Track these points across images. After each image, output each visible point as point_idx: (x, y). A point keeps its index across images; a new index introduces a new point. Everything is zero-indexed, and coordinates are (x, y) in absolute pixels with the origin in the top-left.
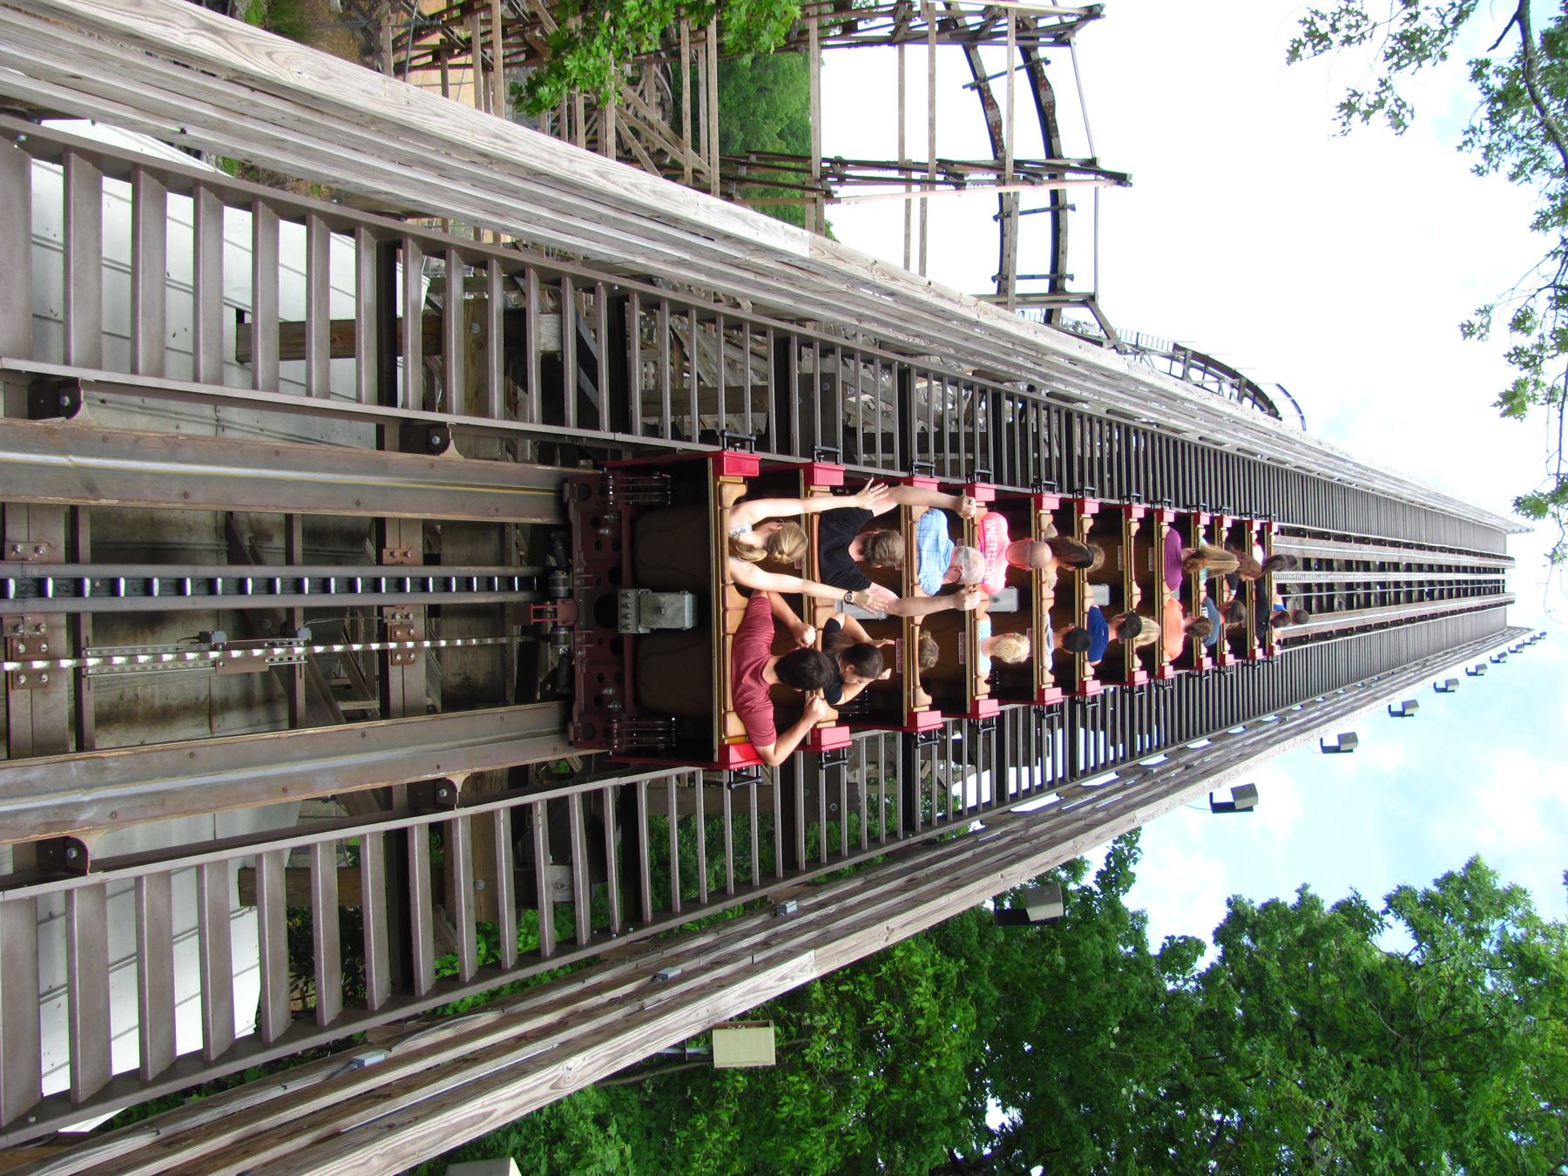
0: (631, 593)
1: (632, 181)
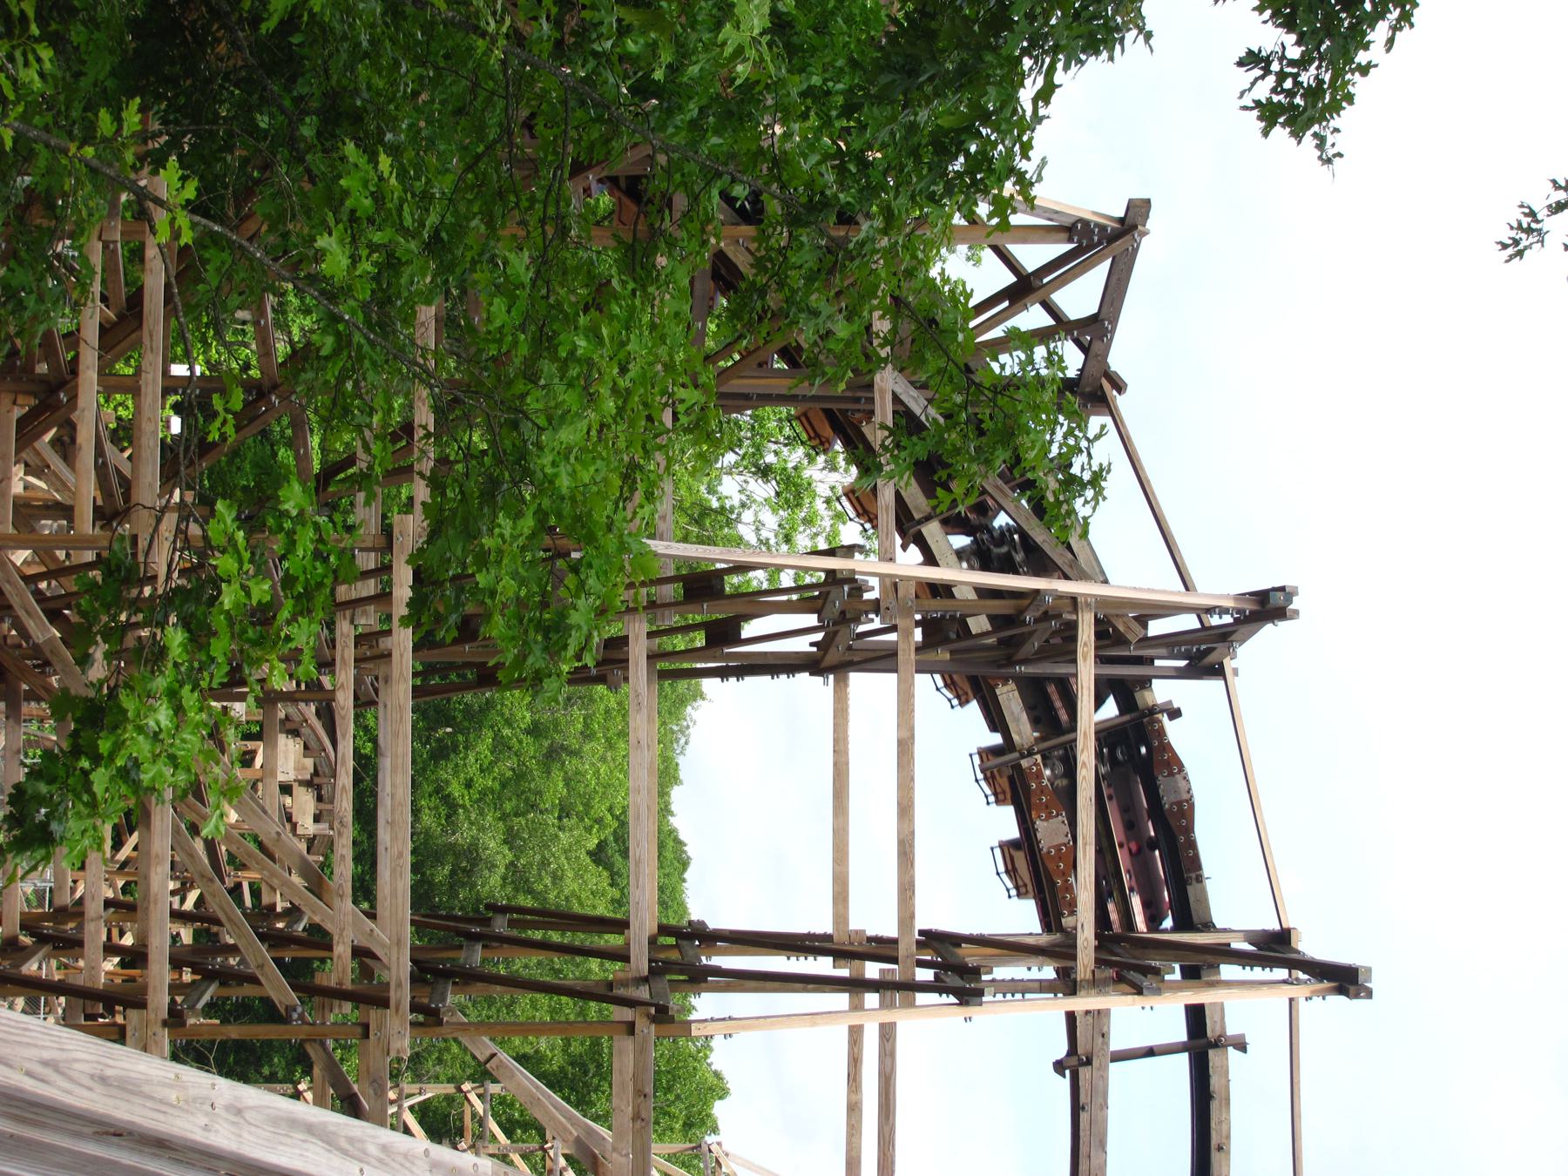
1: (46, 1055)
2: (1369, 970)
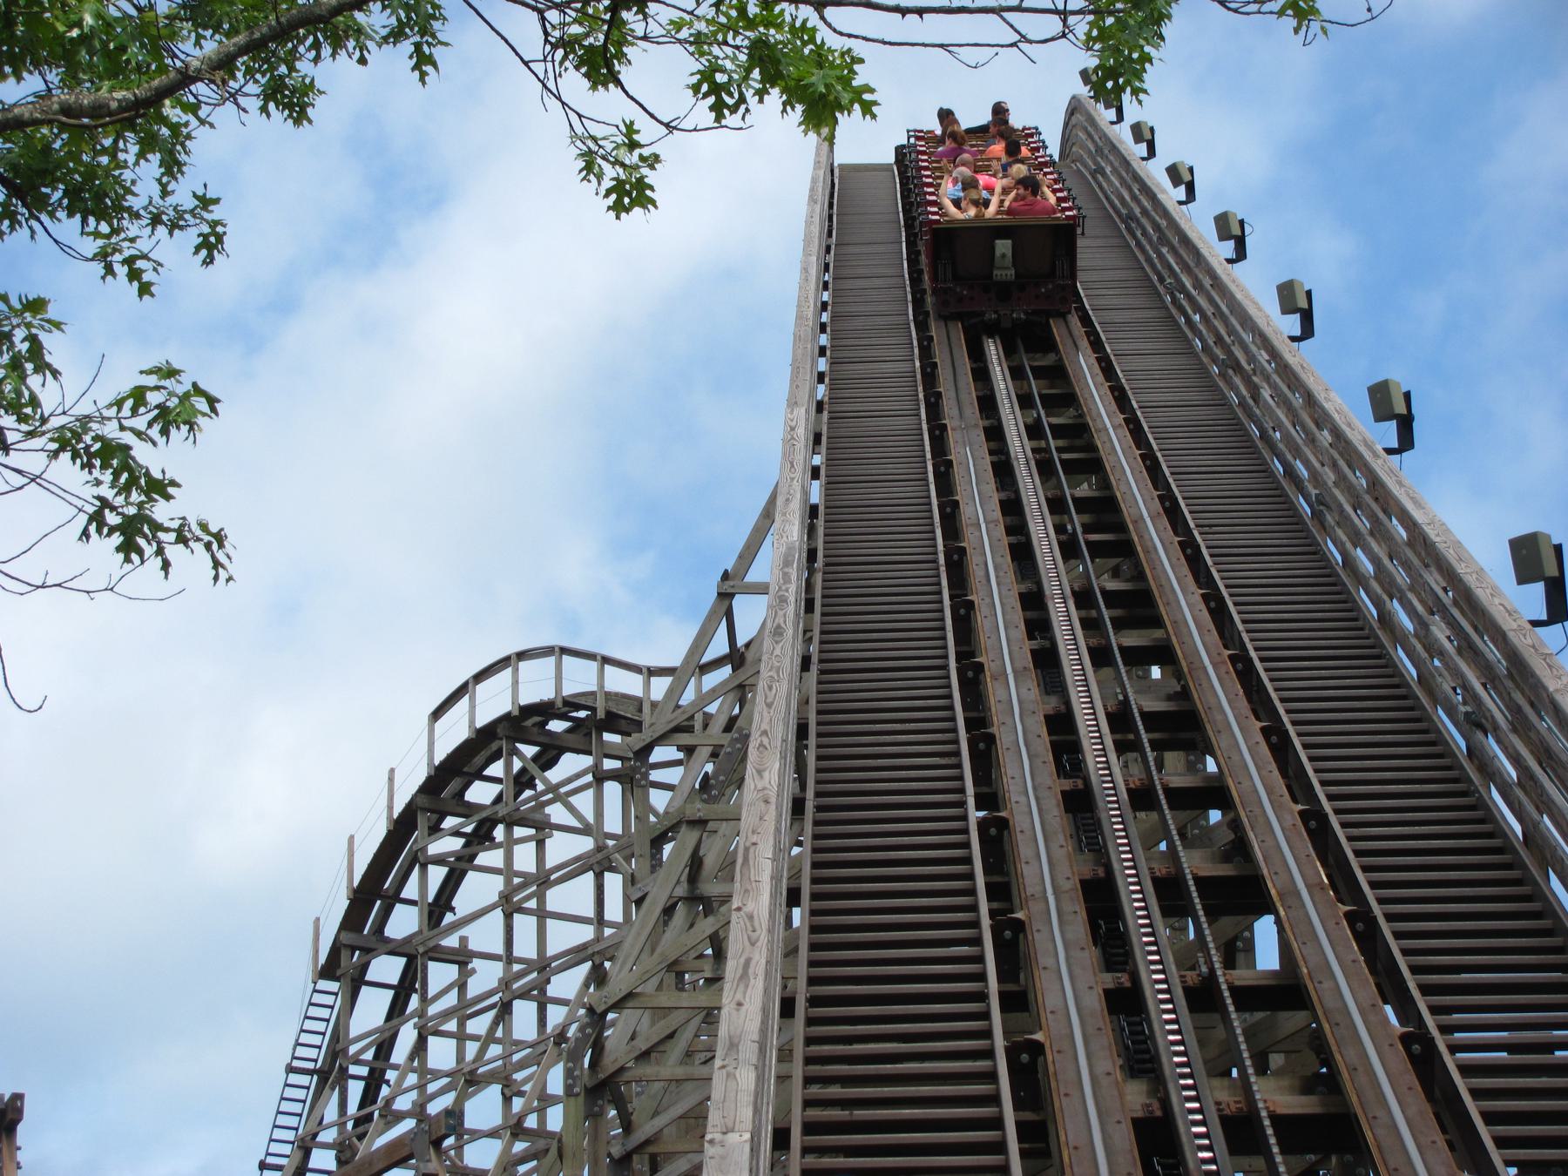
0: (995, 272)
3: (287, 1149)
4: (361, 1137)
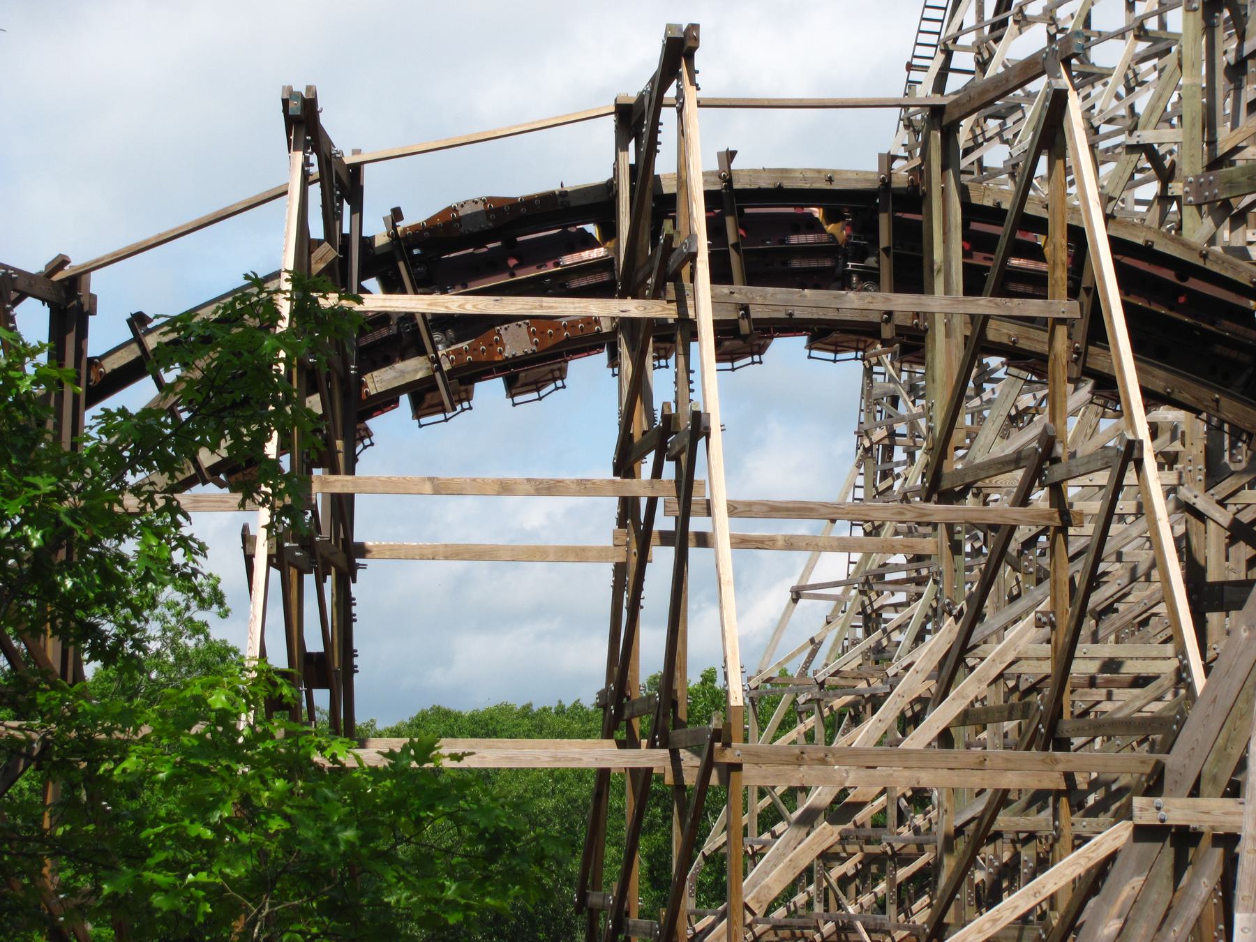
2: (669, 27)
3: (930, 52)
4: (997, 40)
